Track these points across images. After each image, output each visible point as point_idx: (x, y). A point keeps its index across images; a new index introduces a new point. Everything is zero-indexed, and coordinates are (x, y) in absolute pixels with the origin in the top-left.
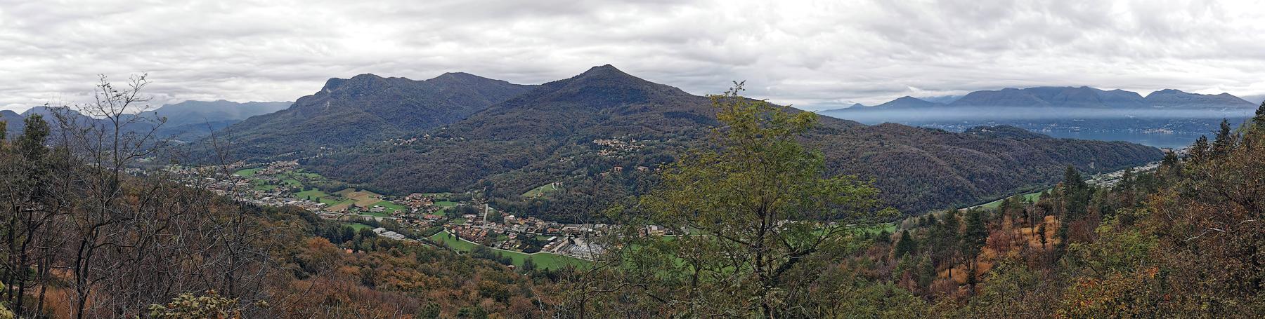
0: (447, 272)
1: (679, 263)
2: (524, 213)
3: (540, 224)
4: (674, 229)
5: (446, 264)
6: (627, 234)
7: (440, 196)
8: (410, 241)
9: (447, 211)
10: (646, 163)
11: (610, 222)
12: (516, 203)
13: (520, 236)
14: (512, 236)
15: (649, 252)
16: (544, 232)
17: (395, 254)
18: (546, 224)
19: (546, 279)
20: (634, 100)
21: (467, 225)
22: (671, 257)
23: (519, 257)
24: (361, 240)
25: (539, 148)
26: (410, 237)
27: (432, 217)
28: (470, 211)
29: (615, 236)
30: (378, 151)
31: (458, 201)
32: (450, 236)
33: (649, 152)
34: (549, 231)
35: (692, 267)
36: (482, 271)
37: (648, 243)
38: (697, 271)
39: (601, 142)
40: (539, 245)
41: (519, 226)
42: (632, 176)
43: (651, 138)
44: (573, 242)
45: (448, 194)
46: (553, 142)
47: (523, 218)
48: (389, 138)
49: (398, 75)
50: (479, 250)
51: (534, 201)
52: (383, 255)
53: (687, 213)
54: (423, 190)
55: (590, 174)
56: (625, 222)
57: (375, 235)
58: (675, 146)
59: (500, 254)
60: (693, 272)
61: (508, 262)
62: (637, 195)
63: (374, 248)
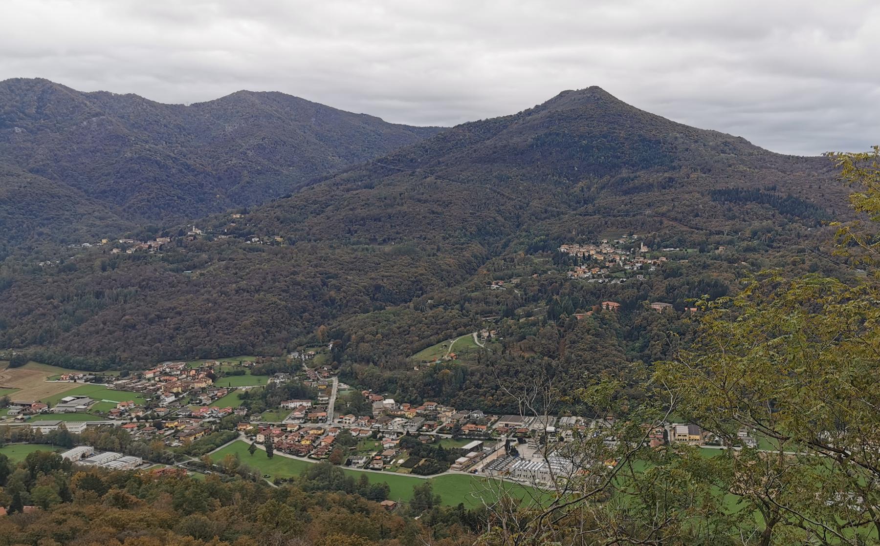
0: (247, 525)
1: (732, 505)
2: (414, 394)
3: (448, 416)
4: (725, 434)
5: (244, 510)
6: (626, 439)
7: (227, 365)
8: (157, 468)
9: (245, 396)
10: (669, 296)
11: (590, 414)
12: (398, 374)
13: (407, 442)
14: (389, 442)
15: (670, 477)
16: (456, 431)
17: (121, 502)
18: (462, 416)
19: (458, 526)
20: (647, 163)
21: (292, 424)
22: (715, 491)
23: (402, 480)
24: (29, 482)
25: (447, 260)
26: (158, 459)
27: (210, 413)
28: (297, 393)
29: (600, 442)
30: (71, 268)
31: (271, 373)
32: (252, 449)
33: (675, 273)
34: (466, 429)
35: (758, 516)
36: (325, 515)
37: (668, 460)
38: (771, 524)
39: (575, 250)
40: (446, 458)
41: (404, 421)
42: (638, 321)
43: (681, 243)
44: (515, 453)
45: (248, 360)
46: (476, 247)
47: (414, 403)
48: (96, 237)
49: (118, 86)
50: (319, 473)
51: (437, 369)
52: (89, 509)
53: (754, 404)
54: (188, 354)
55: (553, 315)
56: (622, 416)
57: (68, 465)
58: (731, 261)
59: (364, 478)
60: (762, 526)
61: (381, 494)
62: (648, 360)
63: (65, 495)
